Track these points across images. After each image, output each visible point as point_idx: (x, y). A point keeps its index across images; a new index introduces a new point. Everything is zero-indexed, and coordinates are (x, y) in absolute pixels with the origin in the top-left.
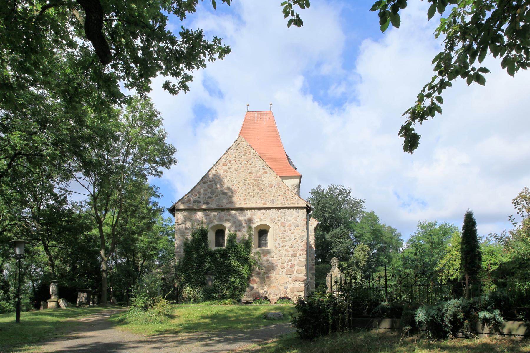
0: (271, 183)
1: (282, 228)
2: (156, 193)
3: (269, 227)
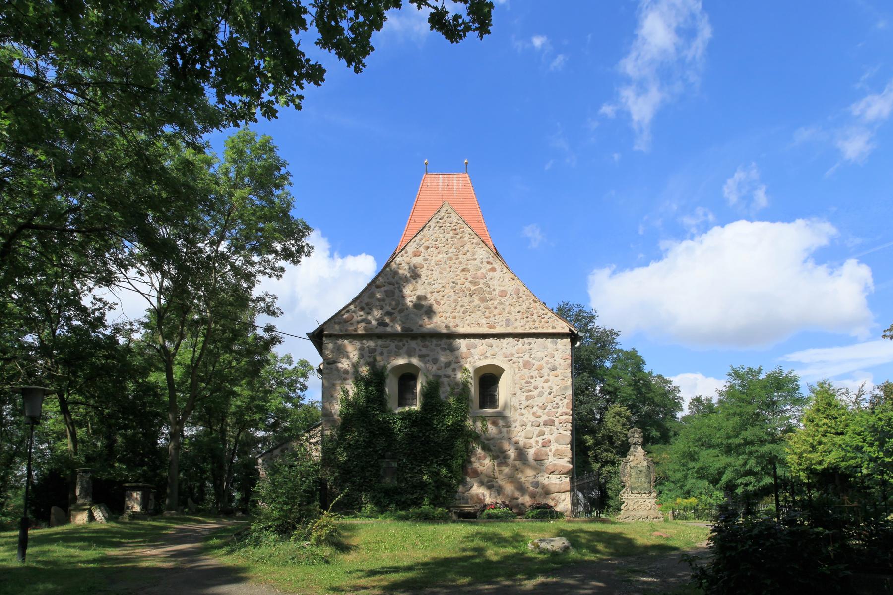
0: (502, 288)
1: (525, 371)
2: (271, 309)
3: (501, 371)
